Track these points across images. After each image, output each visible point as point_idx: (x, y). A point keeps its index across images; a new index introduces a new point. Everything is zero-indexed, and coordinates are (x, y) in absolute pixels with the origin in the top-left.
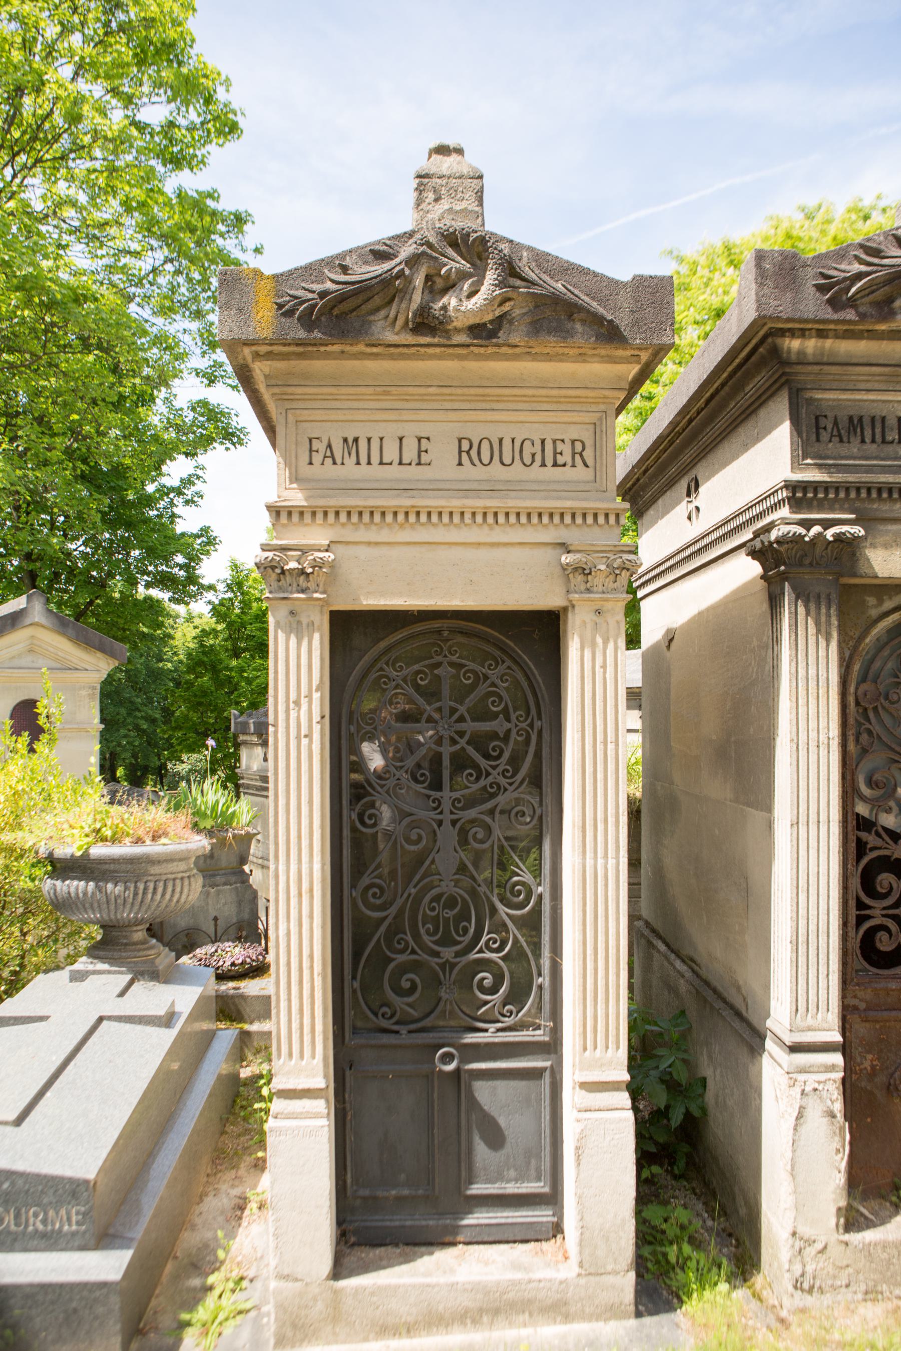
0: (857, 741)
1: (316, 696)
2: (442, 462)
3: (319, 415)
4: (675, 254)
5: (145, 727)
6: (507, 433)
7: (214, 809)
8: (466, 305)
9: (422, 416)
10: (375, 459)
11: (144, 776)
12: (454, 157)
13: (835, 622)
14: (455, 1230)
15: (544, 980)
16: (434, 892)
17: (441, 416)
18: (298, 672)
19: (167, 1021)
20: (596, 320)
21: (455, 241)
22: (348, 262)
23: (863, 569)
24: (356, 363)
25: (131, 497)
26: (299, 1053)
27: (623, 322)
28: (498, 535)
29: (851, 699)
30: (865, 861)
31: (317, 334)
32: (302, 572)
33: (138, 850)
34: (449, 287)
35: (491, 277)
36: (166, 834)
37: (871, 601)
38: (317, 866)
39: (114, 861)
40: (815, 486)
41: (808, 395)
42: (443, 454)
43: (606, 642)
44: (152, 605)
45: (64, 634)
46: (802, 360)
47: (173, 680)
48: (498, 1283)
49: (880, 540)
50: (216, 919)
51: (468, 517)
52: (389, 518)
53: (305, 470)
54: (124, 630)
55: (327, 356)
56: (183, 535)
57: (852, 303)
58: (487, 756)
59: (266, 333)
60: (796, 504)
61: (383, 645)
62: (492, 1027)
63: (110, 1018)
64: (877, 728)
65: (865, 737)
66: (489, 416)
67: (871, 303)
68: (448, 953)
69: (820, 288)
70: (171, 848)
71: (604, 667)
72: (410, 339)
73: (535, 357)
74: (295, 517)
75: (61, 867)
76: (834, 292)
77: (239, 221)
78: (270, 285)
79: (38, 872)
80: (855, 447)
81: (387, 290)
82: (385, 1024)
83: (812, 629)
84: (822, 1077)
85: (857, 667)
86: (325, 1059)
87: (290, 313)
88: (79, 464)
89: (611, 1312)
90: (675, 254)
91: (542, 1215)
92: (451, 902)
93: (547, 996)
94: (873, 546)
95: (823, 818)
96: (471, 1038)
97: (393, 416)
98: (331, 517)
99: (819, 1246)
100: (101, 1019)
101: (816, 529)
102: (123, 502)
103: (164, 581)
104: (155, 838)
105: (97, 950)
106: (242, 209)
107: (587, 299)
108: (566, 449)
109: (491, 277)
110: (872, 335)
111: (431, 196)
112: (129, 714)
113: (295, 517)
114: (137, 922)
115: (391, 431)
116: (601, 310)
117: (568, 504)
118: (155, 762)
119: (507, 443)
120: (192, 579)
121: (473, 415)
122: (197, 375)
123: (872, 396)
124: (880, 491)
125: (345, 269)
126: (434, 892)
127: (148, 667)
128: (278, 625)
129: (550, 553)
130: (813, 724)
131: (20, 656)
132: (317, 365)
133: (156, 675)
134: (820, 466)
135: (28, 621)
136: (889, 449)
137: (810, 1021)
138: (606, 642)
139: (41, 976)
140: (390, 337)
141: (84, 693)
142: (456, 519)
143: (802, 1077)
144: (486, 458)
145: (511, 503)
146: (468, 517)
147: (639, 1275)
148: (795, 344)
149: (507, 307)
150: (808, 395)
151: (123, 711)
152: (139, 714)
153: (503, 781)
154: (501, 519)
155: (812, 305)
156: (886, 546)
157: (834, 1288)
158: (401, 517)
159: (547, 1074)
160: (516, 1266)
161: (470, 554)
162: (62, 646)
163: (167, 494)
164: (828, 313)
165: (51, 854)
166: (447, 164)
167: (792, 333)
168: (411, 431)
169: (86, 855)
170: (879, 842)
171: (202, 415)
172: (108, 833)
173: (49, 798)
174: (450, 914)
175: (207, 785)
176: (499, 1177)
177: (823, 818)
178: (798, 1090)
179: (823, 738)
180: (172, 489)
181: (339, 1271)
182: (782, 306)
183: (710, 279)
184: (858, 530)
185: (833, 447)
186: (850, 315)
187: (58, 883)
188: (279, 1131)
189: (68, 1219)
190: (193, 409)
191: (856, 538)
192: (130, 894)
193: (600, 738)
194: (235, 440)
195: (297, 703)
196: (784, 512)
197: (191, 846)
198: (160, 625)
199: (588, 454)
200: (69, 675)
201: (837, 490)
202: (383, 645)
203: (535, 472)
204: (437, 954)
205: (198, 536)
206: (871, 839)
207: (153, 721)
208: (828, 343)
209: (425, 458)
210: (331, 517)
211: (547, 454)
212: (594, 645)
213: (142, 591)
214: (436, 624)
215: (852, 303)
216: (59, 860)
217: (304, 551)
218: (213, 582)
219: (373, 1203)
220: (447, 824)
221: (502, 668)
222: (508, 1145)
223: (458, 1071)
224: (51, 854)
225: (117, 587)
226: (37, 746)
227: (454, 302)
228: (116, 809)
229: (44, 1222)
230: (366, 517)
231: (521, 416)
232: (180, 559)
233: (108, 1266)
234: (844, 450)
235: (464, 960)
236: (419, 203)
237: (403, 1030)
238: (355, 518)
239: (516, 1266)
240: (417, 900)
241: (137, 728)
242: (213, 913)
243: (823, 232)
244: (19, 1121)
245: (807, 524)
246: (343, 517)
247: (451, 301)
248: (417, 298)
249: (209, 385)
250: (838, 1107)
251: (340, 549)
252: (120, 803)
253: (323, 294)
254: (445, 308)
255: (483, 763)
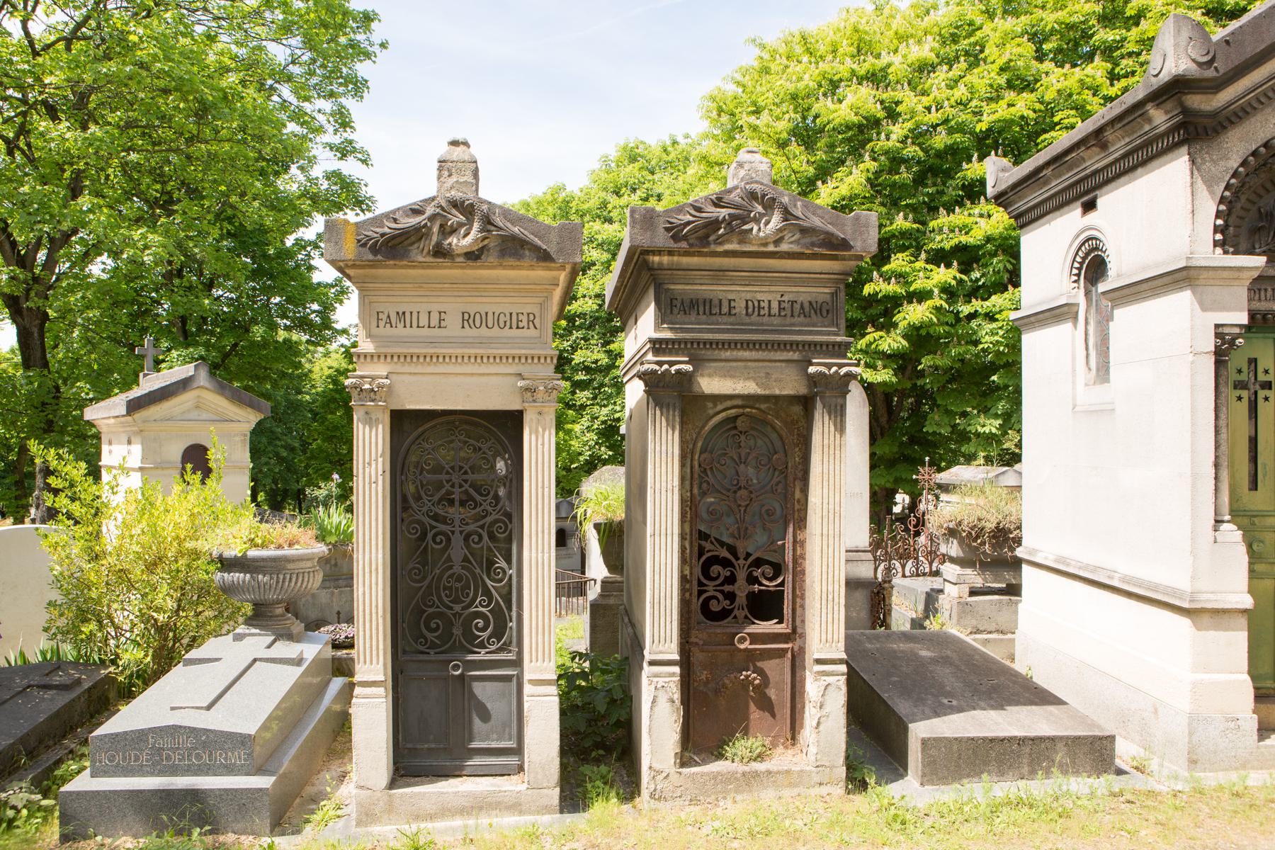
0: (700, 487)
1: (380, 460)
2: (453, 325)
3: (382, 299)
4: (758, 41)
5: (285, 454)
6: (490, 309)
7: (337, 528)
8: (462, 242)
9: (441, 299)
10: (415, 324)
11: (284, 500)
12: (462, 148)
13: (677, 419)
14: (462, 768)
15: (513, 624)
16: (450, 572)
17: (452, 299)
18: (371, 445)
19: (298, 662)
20: (536, 249)
21: (455, 204)
22: (397, 216)
23: (696, 389)
24: (403, 271)
25: (271, 252)
26: (373, 662)
27: (552, 249)
28: (483, 369)
29: (696, 463)
30: (704, 558)
31: (379, 257)
32: (372, 390)
33: (279, 553)
34: (453, 231)
35: (476, 226)
36: (298, 542)
37: (710, 405)
38: (380, 556)
39: (263, 559)
40: (667, 341)
41: (666, 286)
42: (453, 321)
43: (544, 430)
44: (289, 345)
45: (222, 394)
46: (661, 267)
47: (311, 411)
48: (482, 792)
49: (706, 372)
50: (338, 613)
51: (466, 359)
52: (421, 359)
53: (375, 331)
54: (266, 369)
55: (387, 267)
56: (319, 284)
57: (685, 238)
58: (481, 495)
59: (351, 257)
60: (656, 351)
61: (420, 430)
62: (483, 651)
63: (261, 660)
64: (712, 480)
65: (705, 485)
66: (480, 300)
67: (697, 238)
68: (457, 608)
69: (668, 230)
70: (301, 552)
71: (543, 444)
72: (431, 259)
73: (505, 268)
74: (369, 359)
75: (227, 564)
76: (675, 232)
77: (367, 19)
78: (354, 228)
79: (212, 568)
80: (693, 317)
81: (418, 233)
82: (422, 648)
83: (664, 424)
84: (667, 679)
85: (700, 444)
86: (385, 665)
87: (364, 245)
88: (225, 224)
89: (546, 810)
90: (758, 41)
91: (513, 760)
92: (459, 579)
93: (514, 634)
94: (702, 375)
95: (669, 532)
96: (470, 657)
97: (425, 299)
98: (389, 359)
99: (664, 775)
100: (255, 660)
101: (666, 367)
102: (265, 256)
103: (303, 324)
104: (290, 545)
105: (250, 621)
106: (369, 9)
107: (532, 237)
108: (524, 318)
109: (476, 226)
110: (700, 254)
111: (446, 173)
112: (270, 443)
113: (369, 359)
114: (279, 602)
115: (424, 308)
116: (539, 243)
117: (523, 352)
118: (295, 487)
119: (490, 315)
120: (327, 324)
121: (470, 299)
122: (331, 149)
123: (704, 287)
124: (711, 344)
125: (395, 220)
126: (450, 572)
127: (287, 400)
128: (359, 420)
129: (514, 379)
130: (664, 478)
131: (189, 411)
132: (381, 272)
133: (296, 407)
134: (671, 329)
135: (195, 385)
136: (714, 318)
137: (661, 648)
138: (544, 430)
139: (213, 639)
140: (420, 259)
141: (237, 439)
142: (460, 360)
143: (655, 680)
144: (478, 324)
145: (490, 351)
146: (466, 359)
147: (562, 791)
148: (657, 259)
149: (486, 242)
150: (666, 286)
151: (264, 440)
152: (279, 443)
153: (490, 509)
154: (485, 360)
155: (661, 239)
156: (710, 376)
157: (673, 798)
158: (428, 359)
159: (515, 679)
160: (492, 785)
161: (468, 380)
162: (221, 403)
163: (304, 248)
164: (672, 244)
165: (221, 555)
166: (458, 152)
167: (654, 253)
168: (435, 308)
169: (245, 555)
170: (712, 547)
171: (336, 184)
172: (260, 541)
173: (217, 518)
174: (458, 585)
175: (332, 510)
176: (487, 738)
177: (669, 532)
178: (653, 686)
179: (670, 486)
180: (310, 243)
181: (392, 785)
182: (645, 241)
183: (787, 67)
184: (689, 368)
185: (680, 317)
186: (684, 245)
187: (226, 575)
188: (359, 705)
189: (237, 757)
190: (328, 178)
191: (687, 372)
192: (274, 582)
193: (540, 485)
194: (364, 207)
195: (370, 464)
196: (650, 357)
197: (315, 550)
198: (299, 365)
199: (537, 322)
200: (226, 425)
201: (680, 344)
202: (420, 430)
203: (507, 332)
204: (451, 608)
205: (332, 286)
206: (707, 546)
207: (293, 449)
208: (675, 258)
209: (443, 324)
210: (389, 359)
211: (513, 322)
212: (537, 432)
213: (282, 335)
214: (451, 418)
215: (685, 238)
216: (227, 559)
217: (373, 378)
218: (345, 326)
219: (414, 752)
220: (457, 534)
221: (489, 444)
222: (493, 717)
223: (462, 676)
224: (221, 555)
225: (258, 331)
226: (208, 481)
227: (455, 241)
228: (264, 526)
229: (226, 759)
230: (408, 359)
231: (498, 300)
232: (315, 307)
233: (264, 782)
234: (686, 319)
235: (467, 612)
236: (439, 177)
237: (432, 652)
238: (402, 359)
239: (492, 785)
240: (440, 578)
241: (277, 455)
242: (336, 609)
243: (888, 25)
244: (209, 708)
245: (660, 364)
246: (395, 359)
247: (453, 240)
248: (435, 238)
249: (341, 159)
250: (677, 696)
251: (394, 377)
252: (267, 522)
253: (383, 235)
254: (450, 244)
255: (478, 498)
